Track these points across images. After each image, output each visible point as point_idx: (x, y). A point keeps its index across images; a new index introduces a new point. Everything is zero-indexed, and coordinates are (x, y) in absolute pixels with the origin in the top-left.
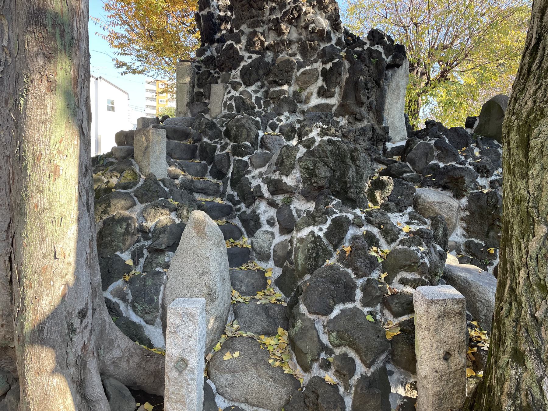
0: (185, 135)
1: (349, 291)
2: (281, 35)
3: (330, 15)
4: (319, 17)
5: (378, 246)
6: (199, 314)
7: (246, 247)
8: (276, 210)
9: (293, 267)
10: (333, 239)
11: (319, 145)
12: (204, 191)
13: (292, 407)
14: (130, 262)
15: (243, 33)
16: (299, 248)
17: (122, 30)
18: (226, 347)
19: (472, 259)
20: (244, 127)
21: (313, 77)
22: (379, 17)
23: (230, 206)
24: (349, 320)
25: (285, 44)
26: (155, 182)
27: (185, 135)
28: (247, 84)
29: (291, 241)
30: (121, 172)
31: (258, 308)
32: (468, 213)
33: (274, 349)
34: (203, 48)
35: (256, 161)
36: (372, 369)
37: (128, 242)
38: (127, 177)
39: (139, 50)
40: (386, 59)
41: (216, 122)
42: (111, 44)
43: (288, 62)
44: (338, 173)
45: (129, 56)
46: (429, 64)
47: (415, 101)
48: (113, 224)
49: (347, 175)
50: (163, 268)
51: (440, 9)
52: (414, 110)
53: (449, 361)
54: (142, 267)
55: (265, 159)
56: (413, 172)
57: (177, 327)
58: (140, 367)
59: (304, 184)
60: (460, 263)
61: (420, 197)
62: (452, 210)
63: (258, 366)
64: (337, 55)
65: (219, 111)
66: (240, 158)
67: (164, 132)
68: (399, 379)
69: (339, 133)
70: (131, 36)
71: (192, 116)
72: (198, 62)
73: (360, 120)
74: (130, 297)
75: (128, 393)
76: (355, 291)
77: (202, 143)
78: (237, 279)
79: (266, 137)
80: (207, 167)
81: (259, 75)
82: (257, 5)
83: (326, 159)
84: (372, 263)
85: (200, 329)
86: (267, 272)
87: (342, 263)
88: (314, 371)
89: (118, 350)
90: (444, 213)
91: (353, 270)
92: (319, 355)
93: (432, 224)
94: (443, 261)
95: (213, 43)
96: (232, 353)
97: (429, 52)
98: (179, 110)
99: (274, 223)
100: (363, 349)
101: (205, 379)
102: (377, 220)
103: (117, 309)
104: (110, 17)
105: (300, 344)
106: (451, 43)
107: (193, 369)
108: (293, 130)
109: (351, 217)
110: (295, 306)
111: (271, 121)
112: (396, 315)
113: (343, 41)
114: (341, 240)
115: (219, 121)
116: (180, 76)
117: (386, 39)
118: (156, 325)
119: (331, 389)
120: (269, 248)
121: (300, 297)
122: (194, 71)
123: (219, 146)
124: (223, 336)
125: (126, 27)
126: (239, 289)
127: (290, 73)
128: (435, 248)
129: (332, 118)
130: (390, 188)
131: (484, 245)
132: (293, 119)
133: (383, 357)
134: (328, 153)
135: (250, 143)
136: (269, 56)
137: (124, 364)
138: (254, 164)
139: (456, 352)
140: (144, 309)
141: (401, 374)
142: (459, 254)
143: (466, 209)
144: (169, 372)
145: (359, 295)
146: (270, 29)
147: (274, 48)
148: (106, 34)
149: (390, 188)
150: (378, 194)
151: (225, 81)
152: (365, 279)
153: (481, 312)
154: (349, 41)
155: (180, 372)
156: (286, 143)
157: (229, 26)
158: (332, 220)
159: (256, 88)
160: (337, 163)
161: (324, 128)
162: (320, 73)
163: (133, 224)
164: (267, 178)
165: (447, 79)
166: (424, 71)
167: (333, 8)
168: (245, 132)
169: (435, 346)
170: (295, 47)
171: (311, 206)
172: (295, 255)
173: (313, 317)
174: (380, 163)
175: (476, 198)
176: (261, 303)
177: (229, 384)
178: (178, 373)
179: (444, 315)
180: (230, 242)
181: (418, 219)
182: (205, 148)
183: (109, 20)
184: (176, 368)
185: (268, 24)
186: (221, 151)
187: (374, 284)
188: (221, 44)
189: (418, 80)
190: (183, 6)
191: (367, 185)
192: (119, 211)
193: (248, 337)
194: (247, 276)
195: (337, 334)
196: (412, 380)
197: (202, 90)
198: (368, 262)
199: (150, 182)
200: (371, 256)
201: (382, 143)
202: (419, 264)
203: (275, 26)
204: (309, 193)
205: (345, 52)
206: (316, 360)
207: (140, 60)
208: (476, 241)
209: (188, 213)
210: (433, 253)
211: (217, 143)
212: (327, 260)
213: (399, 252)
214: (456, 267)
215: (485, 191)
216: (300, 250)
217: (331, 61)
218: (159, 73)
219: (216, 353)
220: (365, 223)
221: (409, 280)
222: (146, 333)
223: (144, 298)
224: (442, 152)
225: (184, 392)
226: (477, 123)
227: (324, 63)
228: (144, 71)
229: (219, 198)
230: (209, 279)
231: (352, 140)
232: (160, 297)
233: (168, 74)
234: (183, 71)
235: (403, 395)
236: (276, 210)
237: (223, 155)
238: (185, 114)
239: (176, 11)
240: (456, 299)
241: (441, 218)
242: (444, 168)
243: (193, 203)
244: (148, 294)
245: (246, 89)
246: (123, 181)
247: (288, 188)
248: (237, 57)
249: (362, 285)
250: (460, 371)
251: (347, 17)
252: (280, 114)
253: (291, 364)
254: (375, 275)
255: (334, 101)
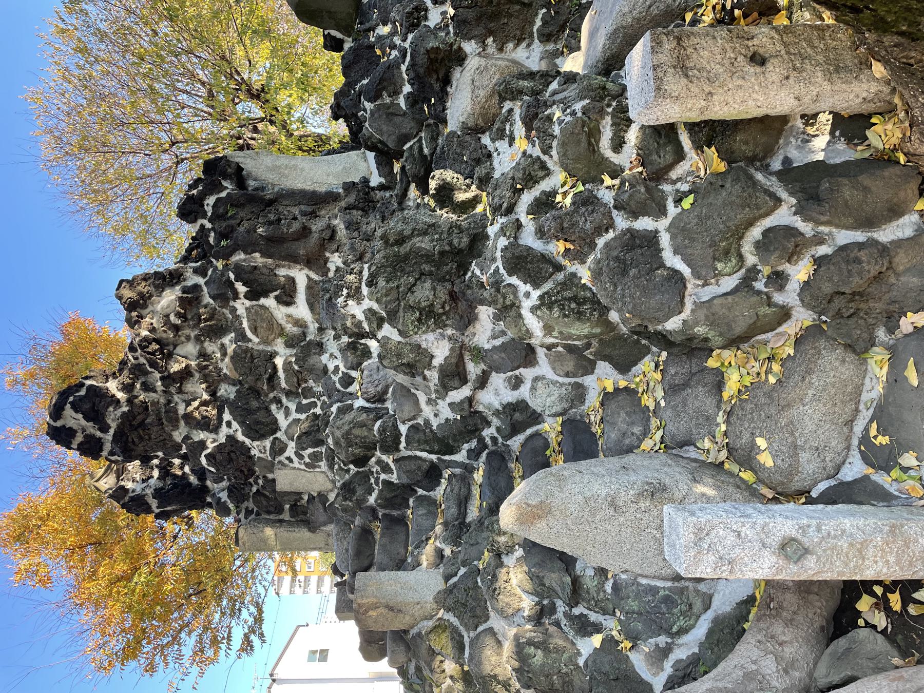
0: (366, 534)
1: (638, 242)
2: (190, 372)
3: (155, 287)
4: (159, 307)
5: (554, 193)
6: (694, 519)
7: (561, 425)
8: (494, 374)
9: (595, 343)
10: (543, 272)
11: (378, 301)
12: (463, 502)
13: (857, 340)
14: (597, 640)
15: (187, 438)
16: (561, 333)
17: (189, 642)
18: (747, 459)
19: (571, 29)
20: (348, 433)
21: (261, 315)
22: (162, 206)
23: (488, 454)
24: (692, 240)
25: (204, 363)
26: (449, 591)
27: (366, 534)
28: (275, 427)
29: (549, 347)
30: (433, 653)
31: (672, 403)
32: (490, 40)
33: (748, 373)
34: (214, 504)
35: (408, 410)
36: (784, 195)
37: (561, 642)
38: (442, 642)
39: (222, 613)
40: (228, 191)
41: (342, 482)
42: (213, 661)
43: (236, 358)
44: (426, 267)
45: (232, 630)
46: (238, 119)
47: (300, 140)
48: (528, 672)
49: (429, 251)
50: (607, 578)
51: (145, 104)
52: (316, 141)
53: (767, 55)
54: (605, 617)
55: (404, 396)
56: (421, 138)
57: (721, 558)
58: (792, 620)
59: (446, 326)
60: (578, 48)
61: (463, 123)
62: (486, 68)
63: (782, 403)
64: (223, 275)
65: (322, 476)
66: (403, 439)
67: (360, 575)
68: (798, 147)
69: (356, 266)
70: (198, 625)
71: (331, 523)
72: (238, 514)
73: (334, 232)
74: (662, 640)
75: (842, 643)
76: (638, 231)
77: (379, 505)
78: (619, 441)
79: (365, 393)
80: (420, 496)
81: (259, 409)
82: (139, 414)
83: (401, 289)
84: (586, 201)
85: (723, 514)
86: (605, 389)
87: (586, 256)
88: (789, 300)
89: (763, 663)
90: (491, 80)
91: (600, 235)
92: (759, 293)
93: (513, 99)
94: (578, 77)
95: (207, 487)
96: (760, 451)
97: (218, 120)
98: (322, 545)
99: (516, 377)
100: (746, 214)
101: (810, 501)
102: (507, 196)
103: (684, 664)
104: (167, 664)
105: (739, 328)
106: (203, 84)
107: (800, 528)
108: (352, 347)
109: (503, 242)
110: (669, 337)
111: (338, 386)
112: (680, 155)
113: (213, 260)
114: (545, 259)
115: (340, 476)
116: (264, 546)
117: (195, 192)
118: (712, 591)
119: (822, 269)
120: (562, 385)
121: (651, 329)
122: (255, 520)
123: (383, 476)
124: (727, 466)
125: (183, 635)
126: (638, 438)
127: (255, 353)
128: (555, 93)
129: (330, 280)
130: (449, 175)
131: (544, 10)
132: (332, 346)
133: (759, 176)
134: (391, 285)
135: (376, 421)
136: (227, 391)
137: (789, 651)
138: (412, 414)
139: (750, 43)
140: (682, 613)
141: (788, 143)
142: (562, 53)
143: (484, 42)
144: (806, 571)
145: (644, 223)
146: (180, 391)
147: (212, 383)
148: (195, 670)
149: (449, 175)
150: (461, 196)
151: (271, 467)
152: (615, 213)
153: (668, 6)
154: (198, 254)
155: (807, 551)
156: (375, 359)
157: (177, 461)
158: (510, 275)
159: (282, 412)
160: (408, 269)
161: (348, 293)
162: (254, 303)
163: (528, 635)
164: (436, 391)
165: (263, 89)
166: (250, 127)
167: (144, 284)
168: (357, 432)
169: (740, 82)
170: (211, 347)
171: (485, 313)
172: (574, 340)
173: (689, 306)
174: (406, 195)
175: (463, 26)
176: (663, 397)
177: (819, 456)
178: (809, 556)
179: (683, 68)
180: (553, 454)
181: (504, 123)
182: (386, 500)
183: (171, 665)
184: (799, 559)
185: (171, 394)
186: (391, 472)
187: (625, 197)
188: (208, 474)
189: (265, 137)
190: (146, 538)
191: (445, 215)
192: (505, 659)
193: (727, 421)
194: (613, 424)
195: (719, 261)
196: (799, 123)
197: (287, 506)
198: (583, 209)
199: (450, 602)
200: (573, 203)
201: (372, 193)
202: (586, 119)
203: (174, 381)
204: (461, 317)
205: (218, 261)
206: (769, 298)
207: (240, 610)
208: (538, 23)
209: (505, 533)
210: (565, 94)
211: (377, 479)
212: (583, 282)
213: (565, 155)
214: (587, 55)
215: (451, 12)
216: (565, 330)
217: (233, 284)
218: (260, 577)
219: (759, 480)
220: (513, 217)
221: (614, 134)
222: (728, 609)
223: (664, 614)
224: (384, 89)
225: (843, 544)
226: (334, 33)
227: (236, 296)
228: (257, 603)
229: (475, 476)
230: (626, 496)
231: (368, 244)
232: (660, 584)
233: (262, 563)
234: (255, 539)
235: (827, 138)
236: (494, 374)
237: (398, 469)
238: (329, 535)
239: (156, 550)
240: (652, 47)
241: (501, 84)
242: (412, 85)
243: (486, 523)
244: (655, 606)
245: (283, 430)
246: (449, 650)
247: (455, 354)
248: (229, 447)
249: (627, 219)
250: (784, 35)
251: (163, 259)
252: (325, 370)
253: (775, 342)
254: (607, 196)
255: (301, 276)
